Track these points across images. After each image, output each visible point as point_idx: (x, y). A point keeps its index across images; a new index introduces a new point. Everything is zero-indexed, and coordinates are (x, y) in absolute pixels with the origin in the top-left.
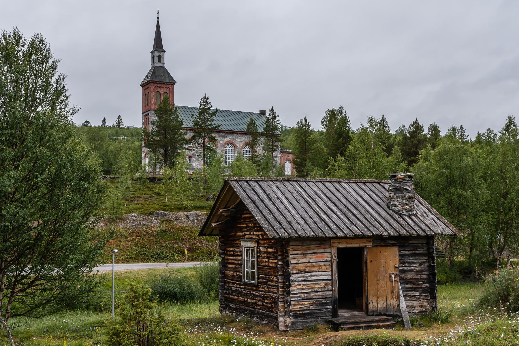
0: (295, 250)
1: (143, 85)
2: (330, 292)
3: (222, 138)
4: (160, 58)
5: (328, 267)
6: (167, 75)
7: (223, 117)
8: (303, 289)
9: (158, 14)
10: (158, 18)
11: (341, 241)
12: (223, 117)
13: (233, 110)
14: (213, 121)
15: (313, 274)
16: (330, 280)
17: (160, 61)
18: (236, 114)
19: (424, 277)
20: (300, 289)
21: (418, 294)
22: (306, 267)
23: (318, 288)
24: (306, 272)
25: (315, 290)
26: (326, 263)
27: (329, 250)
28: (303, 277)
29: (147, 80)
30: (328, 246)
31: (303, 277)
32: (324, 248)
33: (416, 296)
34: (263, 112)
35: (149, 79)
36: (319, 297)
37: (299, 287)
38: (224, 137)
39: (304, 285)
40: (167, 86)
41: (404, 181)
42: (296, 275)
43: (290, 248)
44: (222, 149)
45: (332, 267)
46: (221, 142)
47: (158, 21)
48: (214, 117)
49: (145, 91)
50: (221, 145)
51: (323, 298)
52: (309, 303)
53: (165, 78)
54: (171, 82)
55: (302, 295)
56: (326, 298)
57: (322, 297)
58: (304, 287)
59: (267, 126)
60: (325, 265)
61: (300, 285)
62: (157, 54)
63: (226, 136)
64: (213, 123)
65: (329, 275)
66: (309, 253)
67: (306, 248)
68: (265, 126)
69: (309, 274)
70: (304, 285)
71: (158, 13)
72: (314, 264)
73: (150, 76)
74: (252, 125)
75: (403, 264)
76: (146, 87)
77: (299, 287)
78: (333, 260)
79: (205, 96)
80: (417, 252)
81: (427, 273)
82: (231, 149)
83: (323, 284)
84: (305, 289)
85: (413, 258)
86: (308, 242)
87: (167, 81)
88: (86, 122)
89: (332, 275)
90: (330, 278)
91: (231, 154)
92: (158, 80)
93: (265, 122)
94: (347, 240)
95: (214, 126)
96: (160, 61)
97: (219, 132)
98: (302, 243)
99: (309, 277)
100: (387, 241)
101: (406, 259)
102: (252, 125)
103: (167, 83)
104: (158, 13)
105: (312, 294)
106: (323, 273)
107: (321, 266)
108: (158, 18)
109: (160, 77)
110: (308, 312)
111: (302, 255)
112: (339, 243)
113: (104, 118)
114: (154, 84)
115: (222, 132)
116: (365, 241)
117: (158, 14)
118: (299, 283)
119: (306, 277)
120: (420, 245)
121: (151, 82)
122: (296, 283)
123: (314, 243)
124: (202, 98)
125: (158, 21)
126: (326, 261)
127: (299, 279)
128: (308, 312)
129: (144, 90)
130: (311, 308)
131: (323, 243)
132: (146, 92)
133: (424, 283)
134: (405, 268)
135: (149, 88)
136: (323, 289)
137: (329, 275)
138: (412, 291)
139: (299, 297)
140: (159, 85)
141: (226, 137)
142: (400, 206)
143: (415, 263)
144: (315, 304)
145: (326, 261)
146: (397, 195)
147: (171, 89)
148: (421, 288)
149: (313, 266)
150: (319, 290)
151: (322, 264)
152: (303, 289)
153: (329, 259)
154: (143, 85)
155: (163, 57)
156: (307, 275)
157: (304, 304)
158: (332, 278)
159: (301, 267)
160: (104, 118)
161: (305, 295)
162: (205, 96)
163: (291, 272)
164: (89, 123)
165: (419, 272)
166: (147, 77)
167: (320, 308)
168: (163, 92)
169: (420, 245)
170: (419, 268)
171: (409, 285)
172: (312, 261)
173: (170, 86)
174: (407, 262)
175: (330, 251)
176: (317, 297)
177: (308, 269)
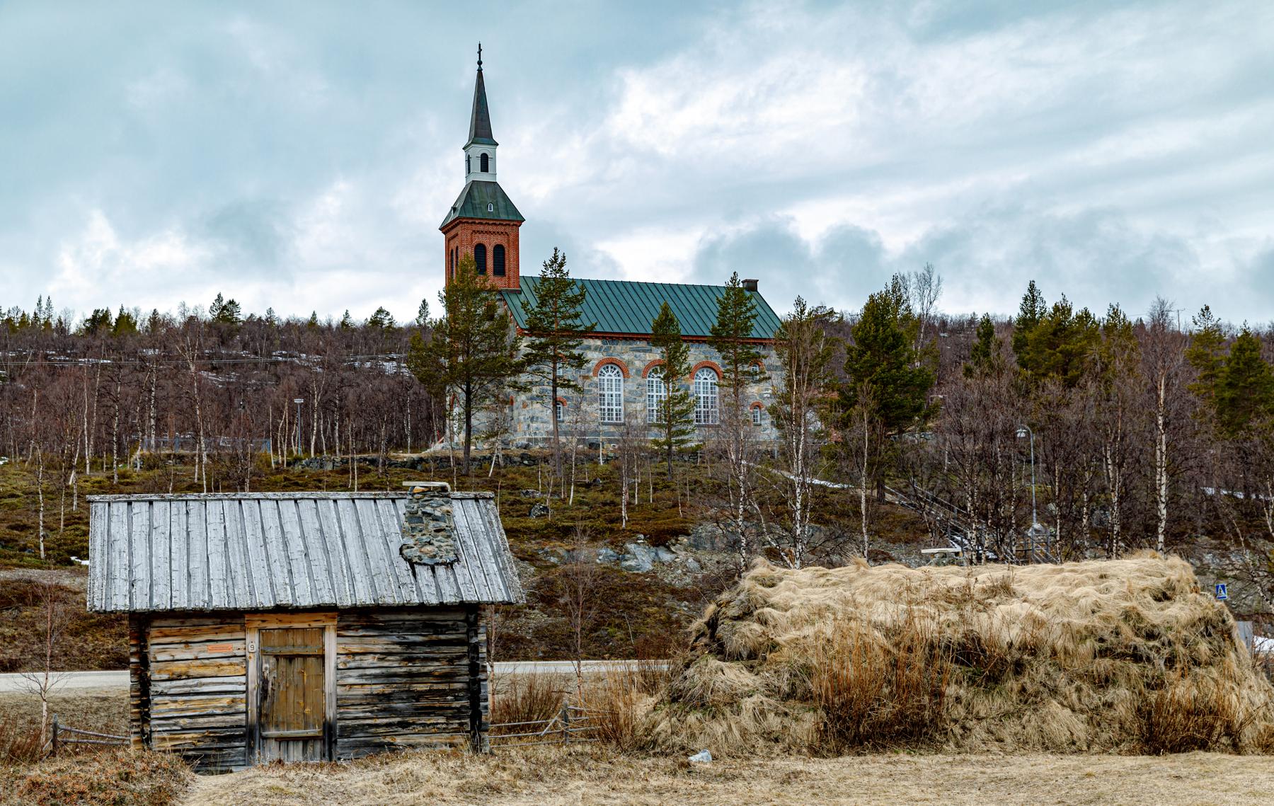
0: (166, 636)
1: (445, 229)
2: (243, 716)
3: (638, 354)
4: (485, 162)
5: (237, 667)
6: (501, 203)
7: (645, 300)
8: (183, 710)
9: (479, 53)
10: (480, 63)
11: (266, 617)
12: (645, 300)
13: (657, 281)
14: (577, 316)
15: (204, 680)
16: (244, 692)
17: (485, 168)
18: (648, 293)
19: (458, 686)
20: (176, 710)
21: (442, 720)
22: (189, 667)
23: (216, 707)
24: (189, 677)
25: (209, 711)
26: (234, 660)
27: (240, 635)
28: (184, 686)
29: (453, 217)
30: (238, 627)
31: (184, 686)
32: (231, 632)
33: (437, 724)
34: (750, 284)
35: (457, 215)
36: (218, 725)
37: (173, 706)
38: (645, 351)
39: (185, 702)
40: (501, 229)
41: (426, 498)
42: (168, 684)
43: (154, 632)
44: (640, 380)
45: (246, 668)
46: (637, 363)
47: (480, 71)
48: (578, 309)
49: (451, 242)
50: (638, 371)
51: (225, 727)
52: (195, 736)
53: (497, 209)
54: (511, 218)
55: (182, 721)
56: (232, 727)
57: (224, 725)
58: (184, 706)
59: (722, 324)
60: (231, 664)
61: (175, 702)
62: (478, 150)
63: (649, 347)
64: (578, 322)
65: (241, 684)
66: (196, 640)
67: (191, 631)
68: (716, 324)
69: (196, 681)
70: (185, 702)
71: (480, 50)
72: (206, 661)
73: (459, 206)
74: (666, 320)
75: (410, 661)
76: (453, 233)
77: (173, 706)
78: (248, 655)
79: (556, 257)
80: (442, 637)
81: (466, 679)
82: (614, 378)
83: (226, 700)
84: (187, 710)
85: (434, 649)
86: (195, 621)
87: (503, 216)
88: (380, 311)
89: (246, 683)
90: (243, 688)
91: (614, 393)
92: (480, 216)
93: (717, 315)
94: (280, 616)
95: (581, 329)
96: (485, 168)
97: (632, 339)
98: (183, 622)
99: (196, 685)
100: (374, 616)
101: (419, 652)
102: (666, 320)
103: (497, 222)
104: (480, 50)
105: (201, 720)
106: (226, 680)
107: (222, 665)
108: (480, 63)
109: (483, 207)
110: (194, 753)
111: (183, 646)
112: (263, 621)
113: (424, 301)
114: (469, 226)
115: (638, 339)
116: (323, 618)
117: (479, 53)
118: (174, 698)
119: (190, 686)
120: (450, 623)
121: (461, 222)
122: (167, 698)
123: (209, 622)
124: (548, 262)
125: (480, 71)
126: (235, 656)
127: (173, 691)
128: (194, 753)
129: (448, 241)
130: (200, 745)
131: (228, 621)
132: (453, 245)
133: (457, 699)
134: (414, 669)
135: (457, 235)
136: (226, 711)
137: (241, 684)
138: (428, 714)
139: (175, 725)
140: (481, 228)
141: (650, 351)
142: (416, 548)
143: (437, 660)
144: (208, 739)
145: (235, 656)
146: (413, 525)
147: (511, 237)
148: (451, 708)
149: (205, 665)
150: (218, 711)
151: (225, 661)
152: (183, 710)
153: (241, 653)
154: (445, 229)
155: (494, 159)
156: (190, 682)
157: (185, 739)
158: (247, 688)
159: (179, 668)
160: (424, 301)
161: (187, 720)
162: (556, 257)
163: (156, 677)
164: (388, 314)
165: (448, 677)
166: (454, 209)
167: (219, 745)
168: (493, 244)
169: (450, 623)
170: (447, 669)
171: (423, 703)
172: (201, 655)
173: (508, 230)
174: (418, 658)
175: (243, 637)
176: (214, 725)
177: (193, 672)
